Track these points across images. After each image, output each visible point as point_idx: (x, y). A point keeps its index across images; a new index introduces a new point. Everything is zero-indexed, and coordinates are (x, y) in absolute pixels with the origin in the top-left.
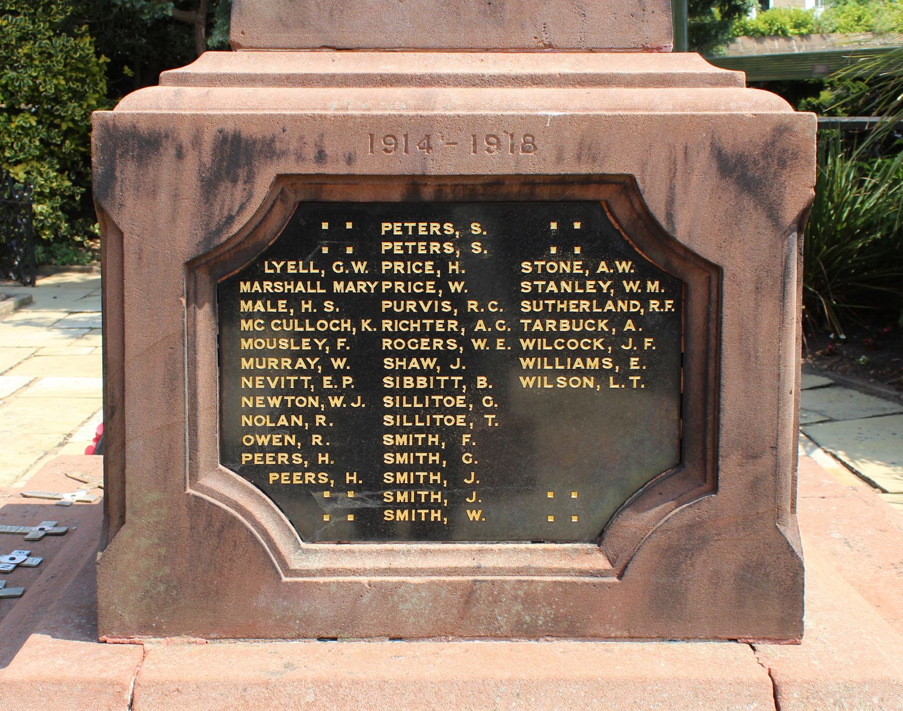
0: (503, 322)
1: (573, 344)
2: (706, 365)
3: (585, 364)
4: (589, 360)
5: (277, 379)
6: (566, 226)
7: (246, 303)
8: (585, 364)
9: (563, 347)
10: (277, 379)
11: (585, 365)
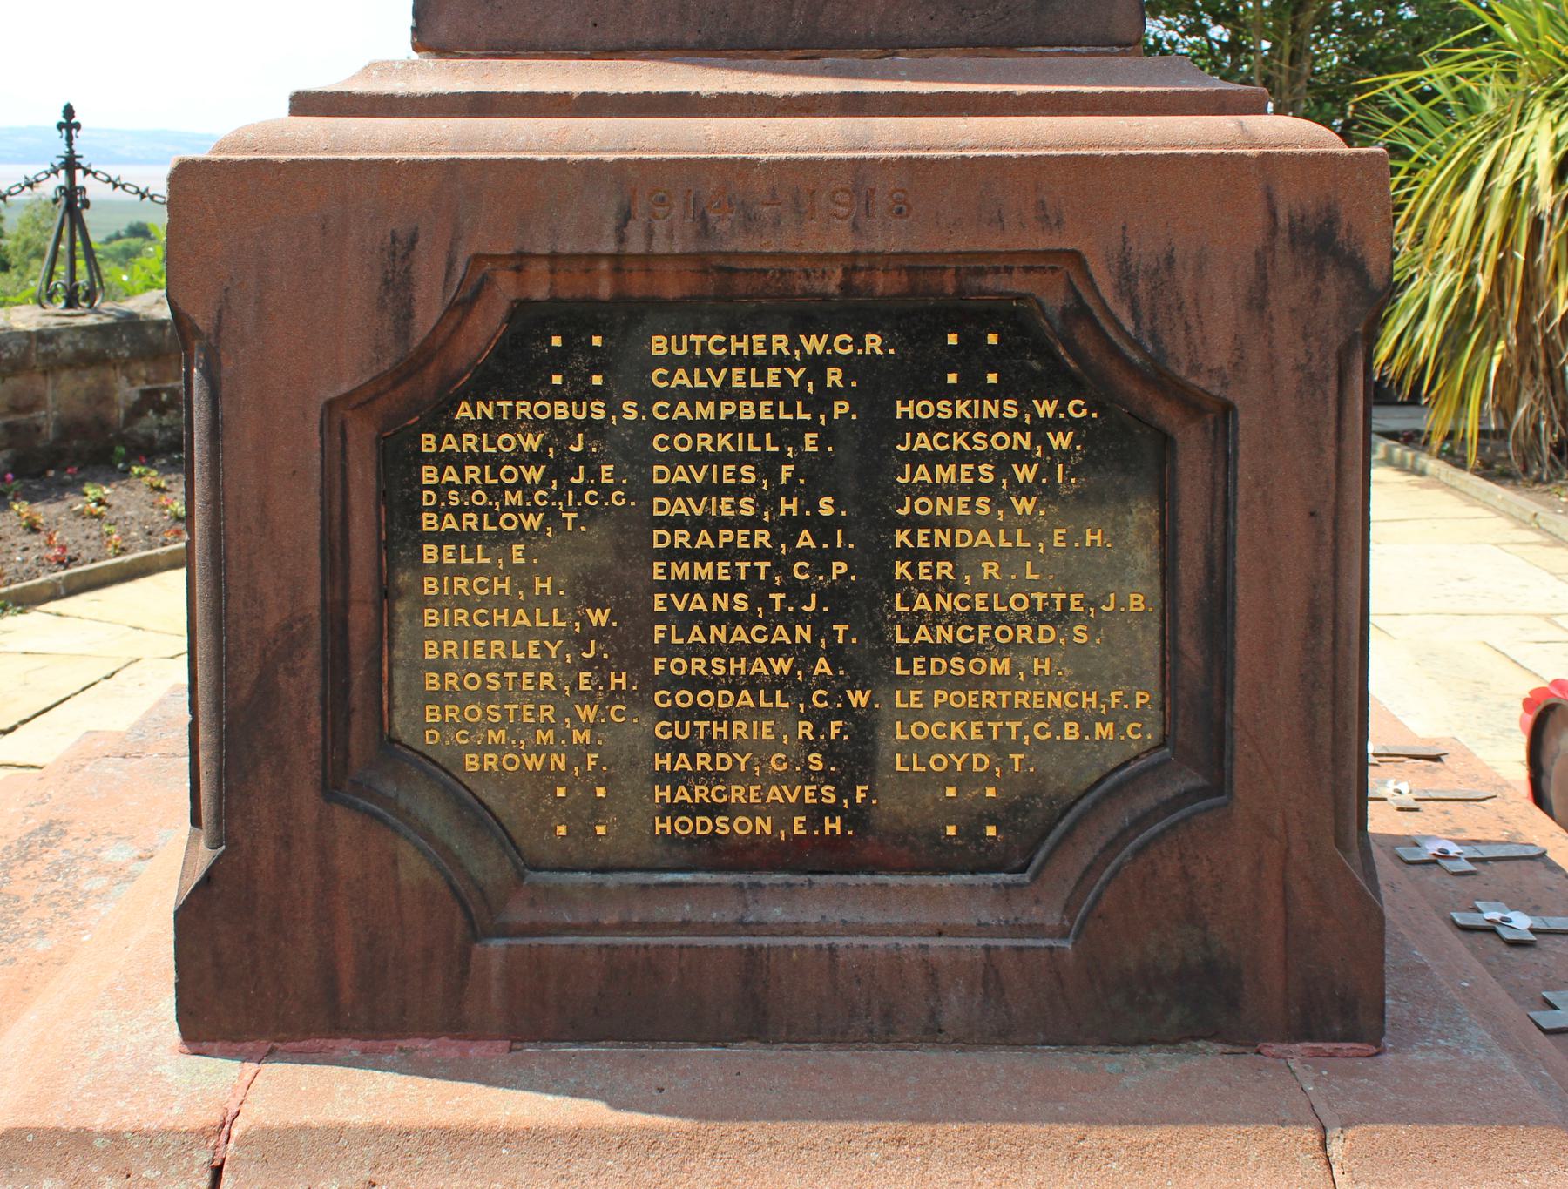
0: (1082, 403)
1: (683, 443)
2: (1226, 492)
3: (933, 475)
4: (939, 468)
5: (705, 468)
6: (972, 342)
7: (680, 567)
8: (933, 475)
9: (667, 448)
10: (705, 468)
11: (933, 476)
